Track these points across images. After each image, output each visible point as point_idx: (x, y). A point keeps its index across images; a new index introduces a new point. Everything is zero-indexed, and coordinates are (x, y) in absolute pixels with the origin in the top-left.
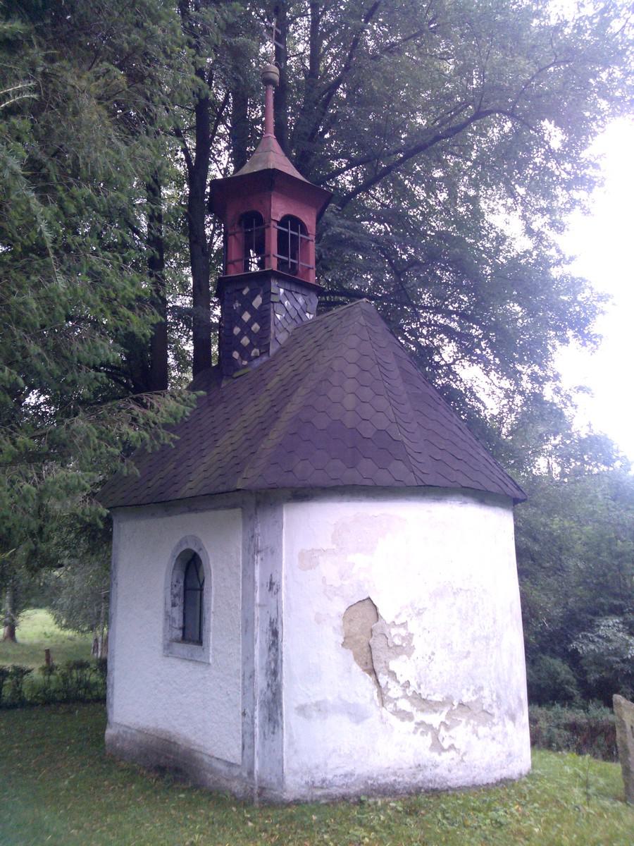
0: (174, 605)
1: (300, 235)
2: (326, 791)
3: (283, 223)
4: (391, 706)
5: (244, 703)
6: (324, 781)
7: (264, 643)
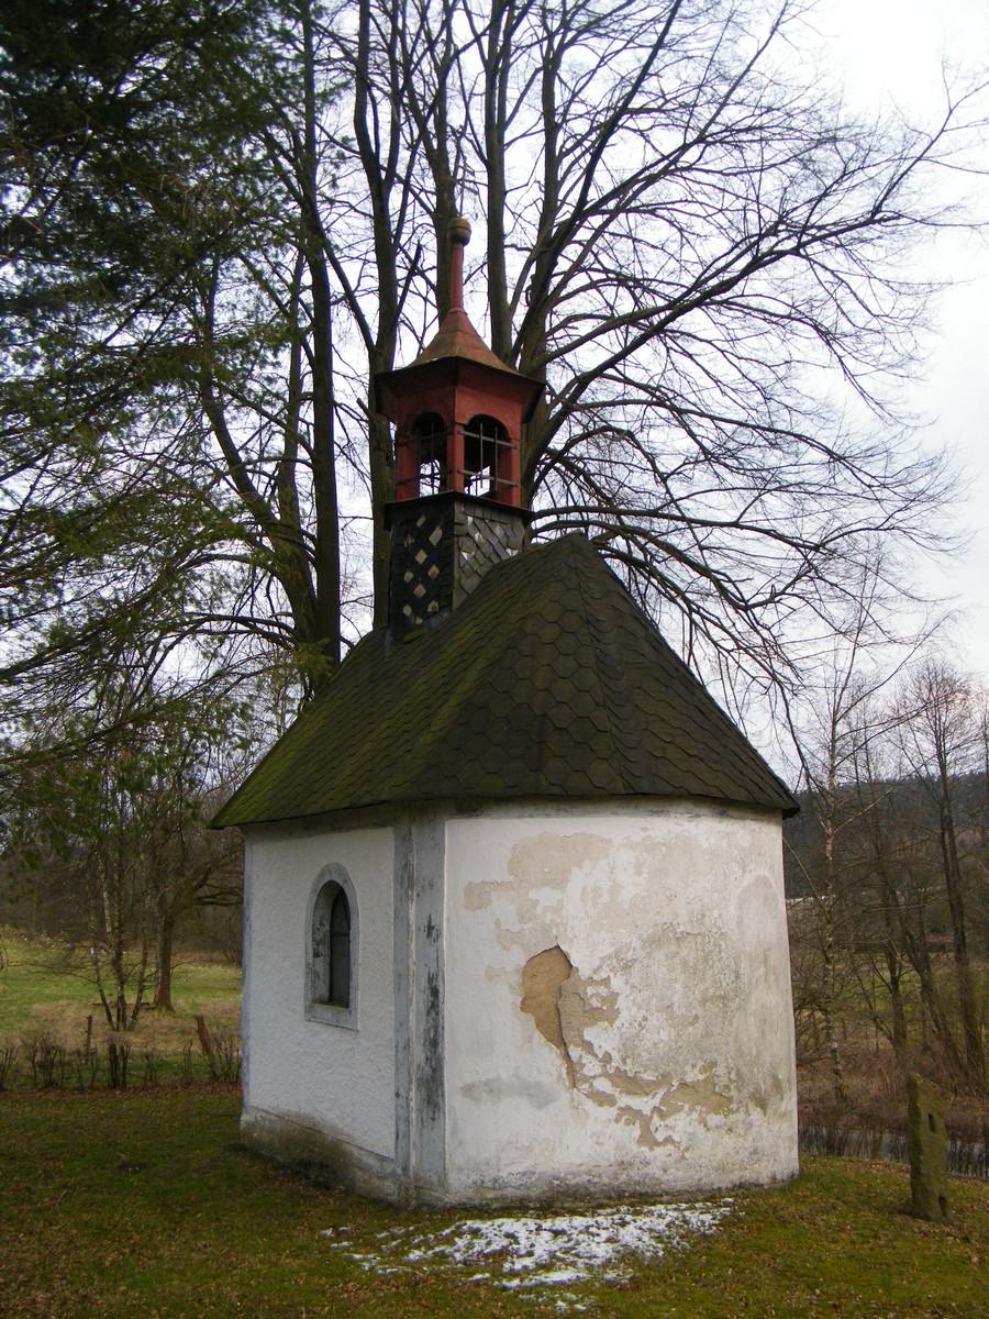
0: (316, 955)
1: (499, 442)
2: (499, 1193)
3: (473, 425)
4: (586, 1086)
5: (397, 1080)
6: (496, 1181)
7: (421, 1004)
